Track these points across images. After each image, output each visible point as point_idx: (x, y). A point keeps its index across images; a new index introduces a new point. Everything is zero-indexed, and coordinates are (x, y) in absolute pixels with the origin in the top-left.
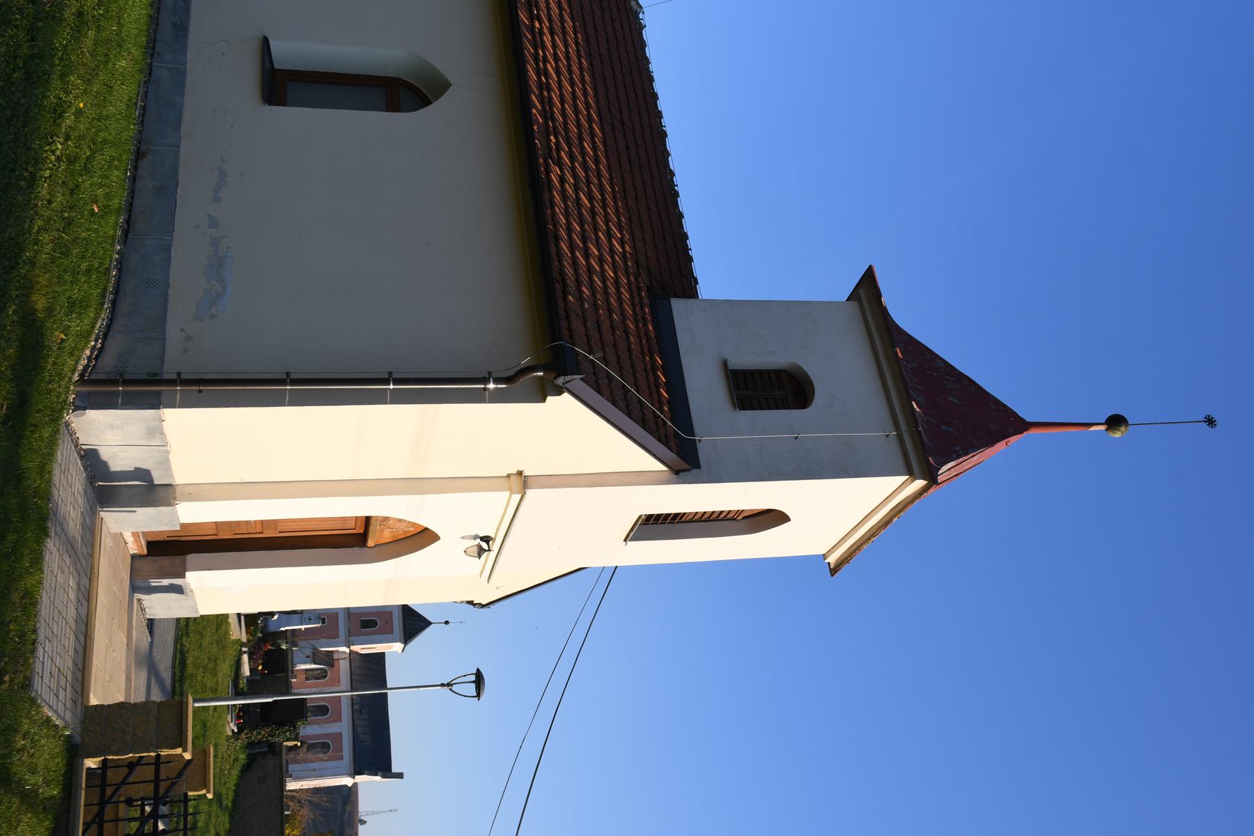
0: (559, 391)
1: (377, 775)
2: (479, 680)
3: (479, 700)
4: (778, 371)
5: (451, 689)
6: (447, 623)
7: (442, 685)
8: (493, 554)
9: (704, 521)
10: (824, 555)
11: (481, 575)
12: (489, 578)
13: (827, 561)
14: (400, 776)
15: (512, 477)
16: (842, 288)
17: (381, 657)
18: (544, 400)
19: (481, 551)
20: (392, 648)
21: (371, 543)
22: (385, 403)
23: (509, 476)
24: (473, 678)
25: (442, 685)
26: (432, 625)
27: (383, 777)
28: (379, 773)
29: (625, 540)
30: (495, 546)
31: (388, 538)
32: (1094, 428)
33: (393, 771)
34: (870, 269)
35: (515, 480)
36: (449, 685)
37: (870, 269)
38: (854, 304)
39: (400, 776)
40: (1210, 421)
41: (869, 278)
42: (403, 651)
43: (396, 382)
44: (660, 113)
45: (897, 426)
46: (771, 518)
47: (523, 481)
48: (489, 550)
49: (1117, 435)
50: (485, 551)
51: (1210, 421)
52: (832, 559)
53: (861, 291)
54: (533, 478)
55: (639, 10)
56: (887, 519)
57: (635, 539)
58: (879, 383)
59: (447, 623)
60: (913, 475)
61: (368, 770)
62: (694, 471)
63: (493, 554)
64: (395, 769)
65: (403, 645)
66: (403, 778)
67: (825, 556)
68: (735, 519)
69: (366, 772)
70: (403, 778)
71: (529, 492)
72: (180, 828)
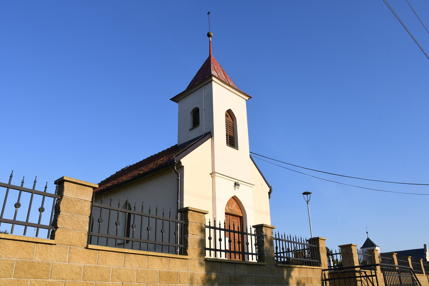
0: (180, 163)
1: (426, 253)
2: (306, 193)
3: (311, 193)
4: (193, 117)
5: (309, 201)
6: (367, 233)
7: (308, 204)
8: (239, 182)
9: (234, 131)
10: (246, 101)
11: (252, 187)
12: (253, 185)
13: (247, 99)
14: (425, 246)
15: (212, 176)
16: (175, 105)
17: (382, 255)
18: (183, 166)
19: (238, 185)
20: (379, 250)
21: (241, 215)
22: (183, 203)
23: (212, 177)
24: (305, 196)
25: (308, 204)
26: (369, 237)
27: (426, 251)
28: (425, 253)
29: (238, 150)
30: (237, 181)
31: (239, 210)
32: (211, 40)
33: (424, 248)
34: (171, 99)
35: (213, 175)
36: (307, 202)
37: (171, 99)
38: (179, 102)
39: (425, 246)
40: (209, 13)
41: (173, 99)
42: (379, 247)
43: (178, 200)
44: (147, 158)
45: (202, 87)
46: (230, 114)
47: (213, 174)
48: (238, 183)
49: (212, 34)
50: (238, 184)
51: (209, 13)
52: (247, 98)
53: (176, 101)
54: (213, 171)
55: (127, 167)
56: (228, 85)
57: (238, 148)
58: (194, 93)
59: (367, 233)
60: (212, 80)
61: (424, 257)
62: (211, 133)
63: (239, 182)
64: (423, 247)
65: (376, 247)
66: (426, 245)
67: (246, 100)
68: (233, 123)
69: (425, 257)
70: (426, 245)
71: (215, 171)
72: (360, 279)
